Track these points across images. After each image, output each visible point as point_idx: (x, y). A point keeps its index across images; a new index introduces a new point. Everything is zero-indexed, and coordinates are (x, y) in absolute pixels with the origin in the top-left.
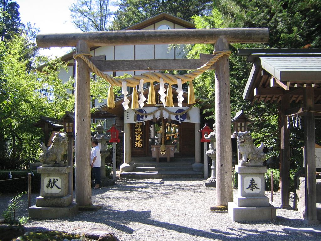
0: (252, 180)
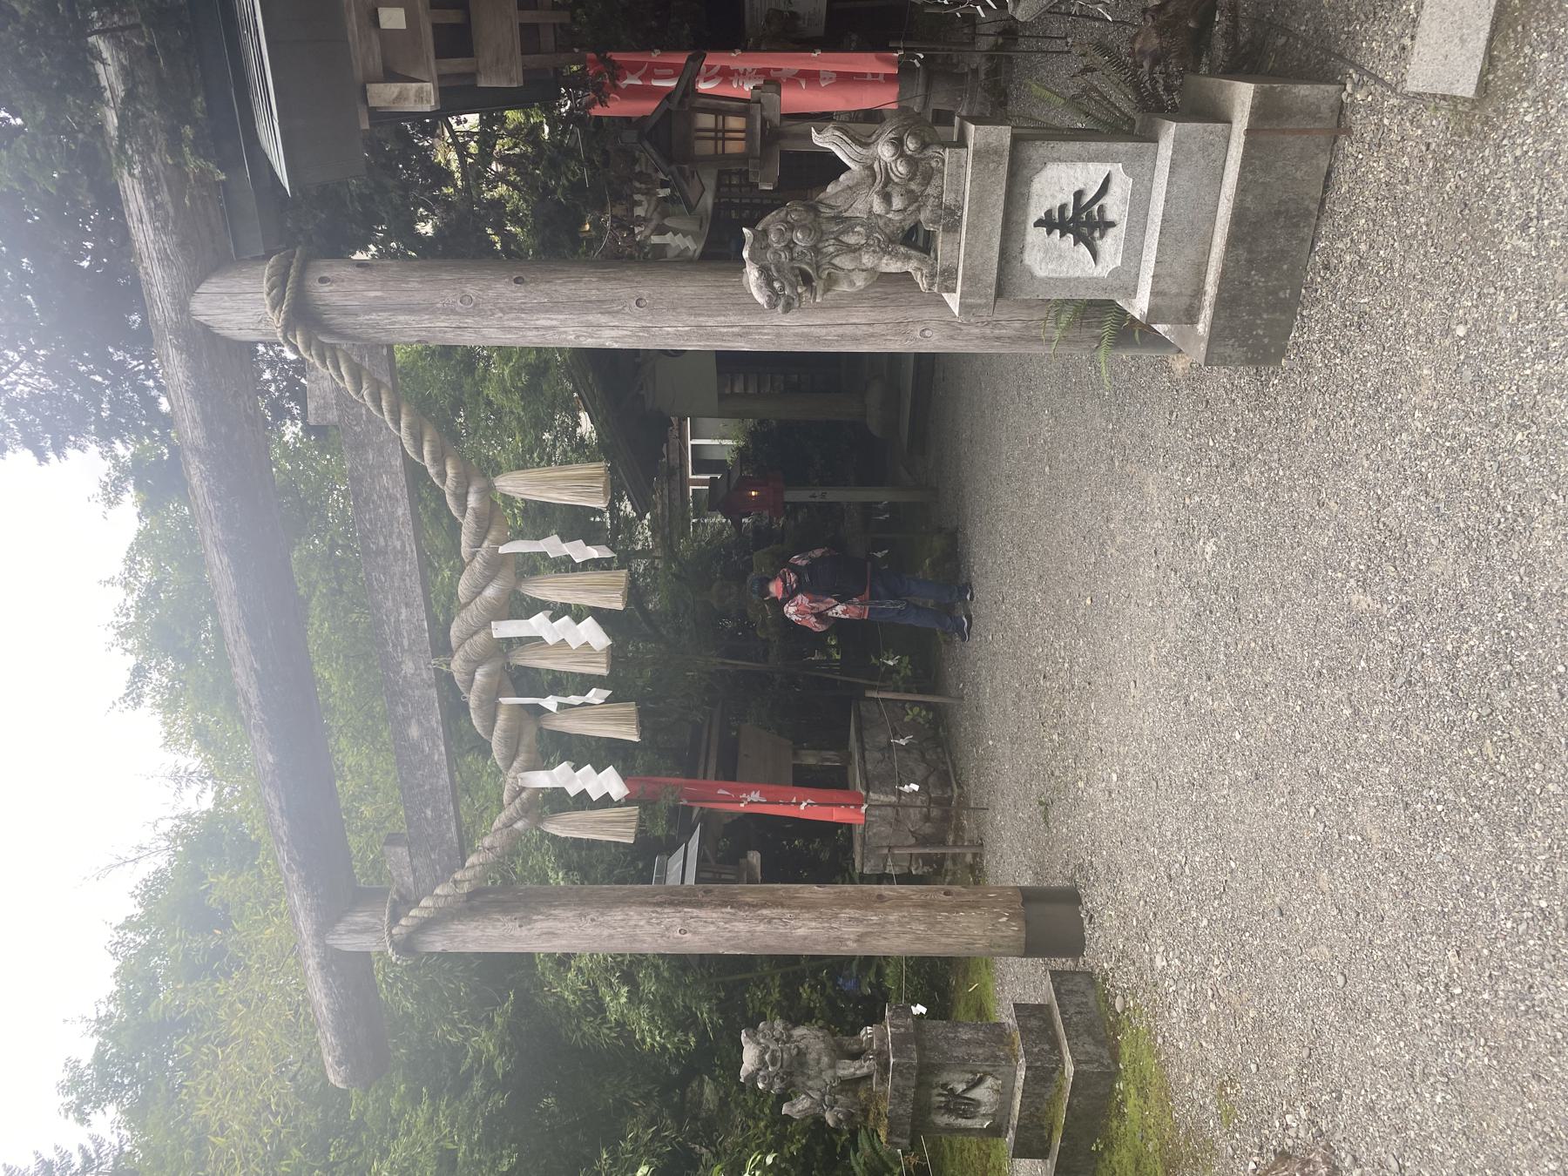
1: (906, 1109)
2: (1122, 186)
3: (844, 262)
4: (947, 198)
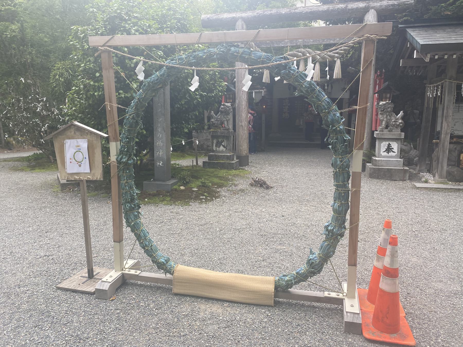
0: (389, 145)
1: (219, 134)
2: (394, 154)
3: (385, 116)
4: (393, 130)
